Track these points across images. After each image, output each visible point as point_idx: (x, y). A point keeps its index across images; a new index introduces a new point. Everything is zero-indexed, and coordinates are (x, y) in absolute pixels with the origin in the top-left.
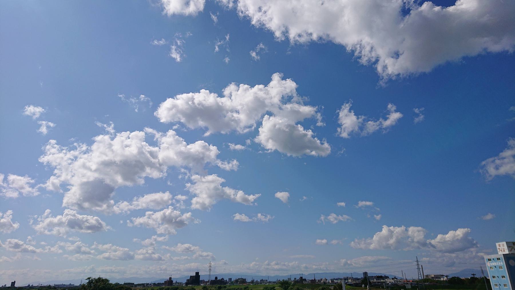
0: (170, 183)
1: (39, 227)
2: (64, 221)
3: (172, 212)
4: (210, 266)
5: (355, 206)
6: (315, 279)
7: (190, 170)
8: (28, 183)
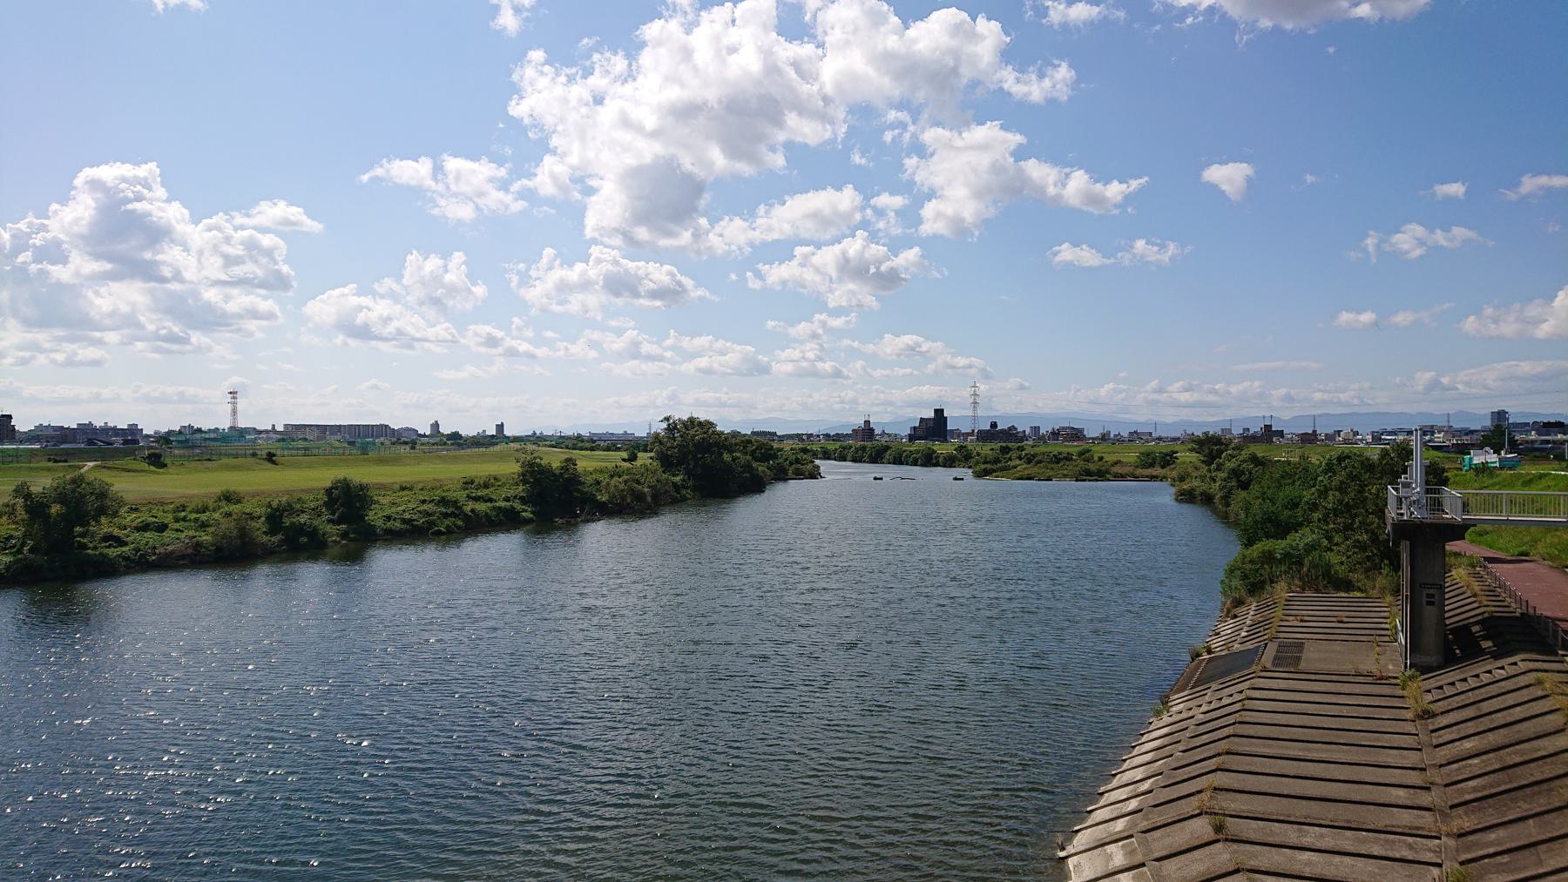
0: (861, 158)
1: (534, 294)
2: (594, 277)
3: (864, 247)
4: (975, 395)
5: (1507, 192)
6: (1315, 431)
7: (915, 114)
8: (491, 180)
